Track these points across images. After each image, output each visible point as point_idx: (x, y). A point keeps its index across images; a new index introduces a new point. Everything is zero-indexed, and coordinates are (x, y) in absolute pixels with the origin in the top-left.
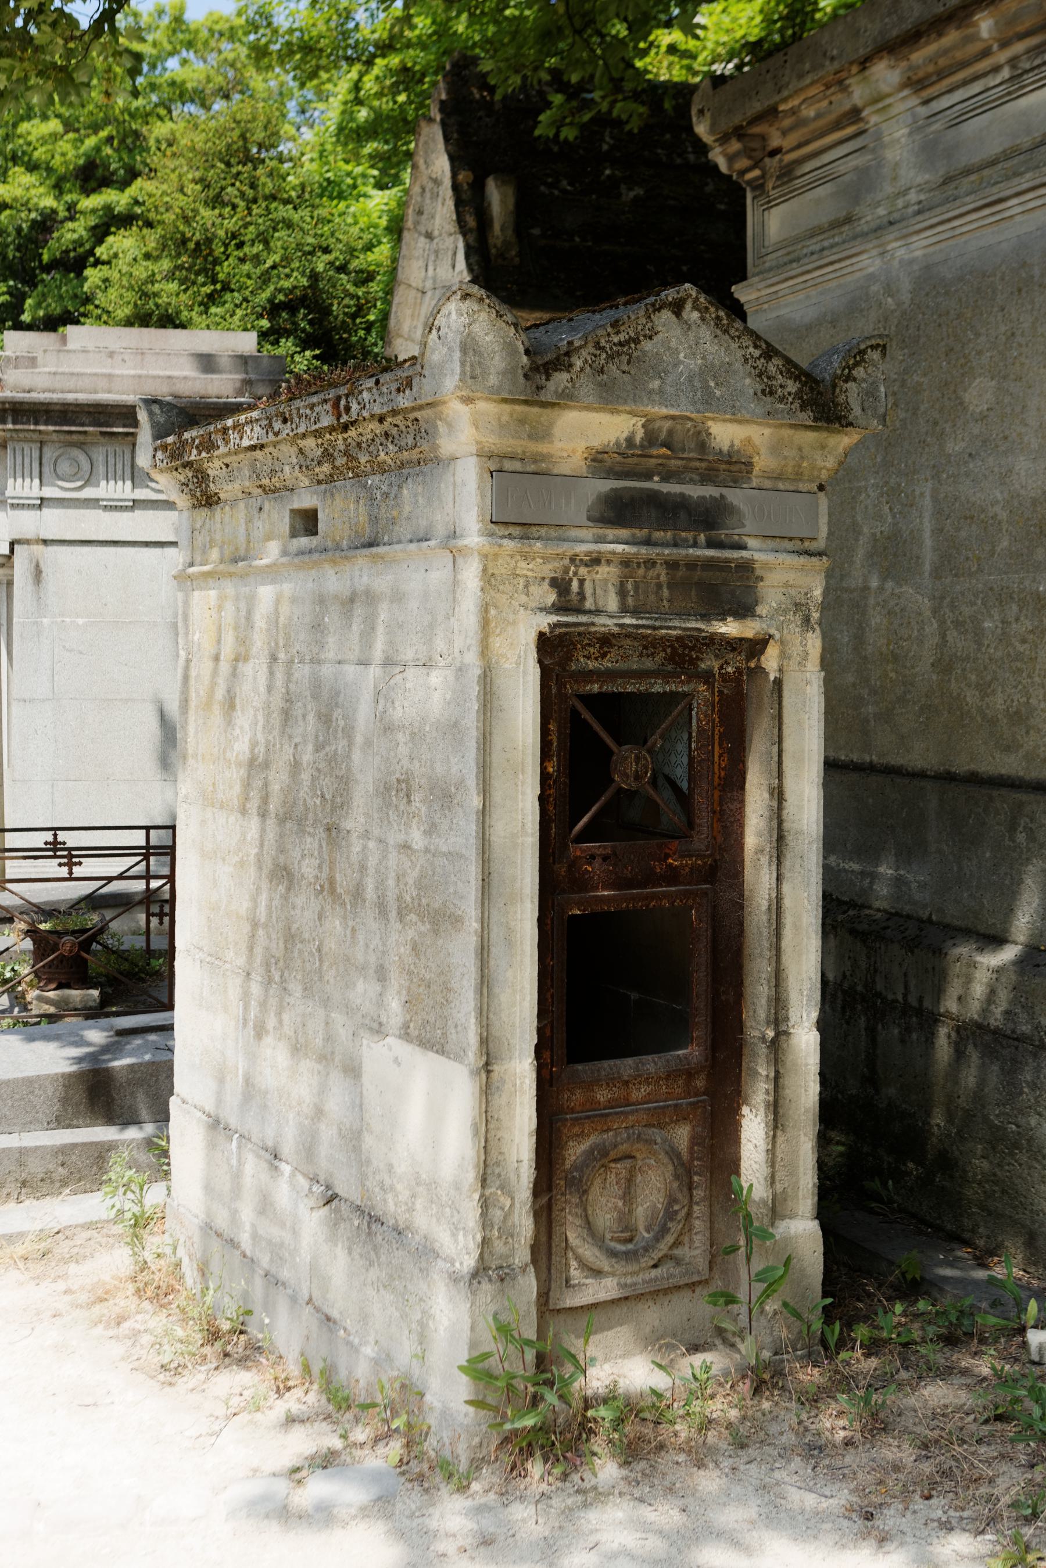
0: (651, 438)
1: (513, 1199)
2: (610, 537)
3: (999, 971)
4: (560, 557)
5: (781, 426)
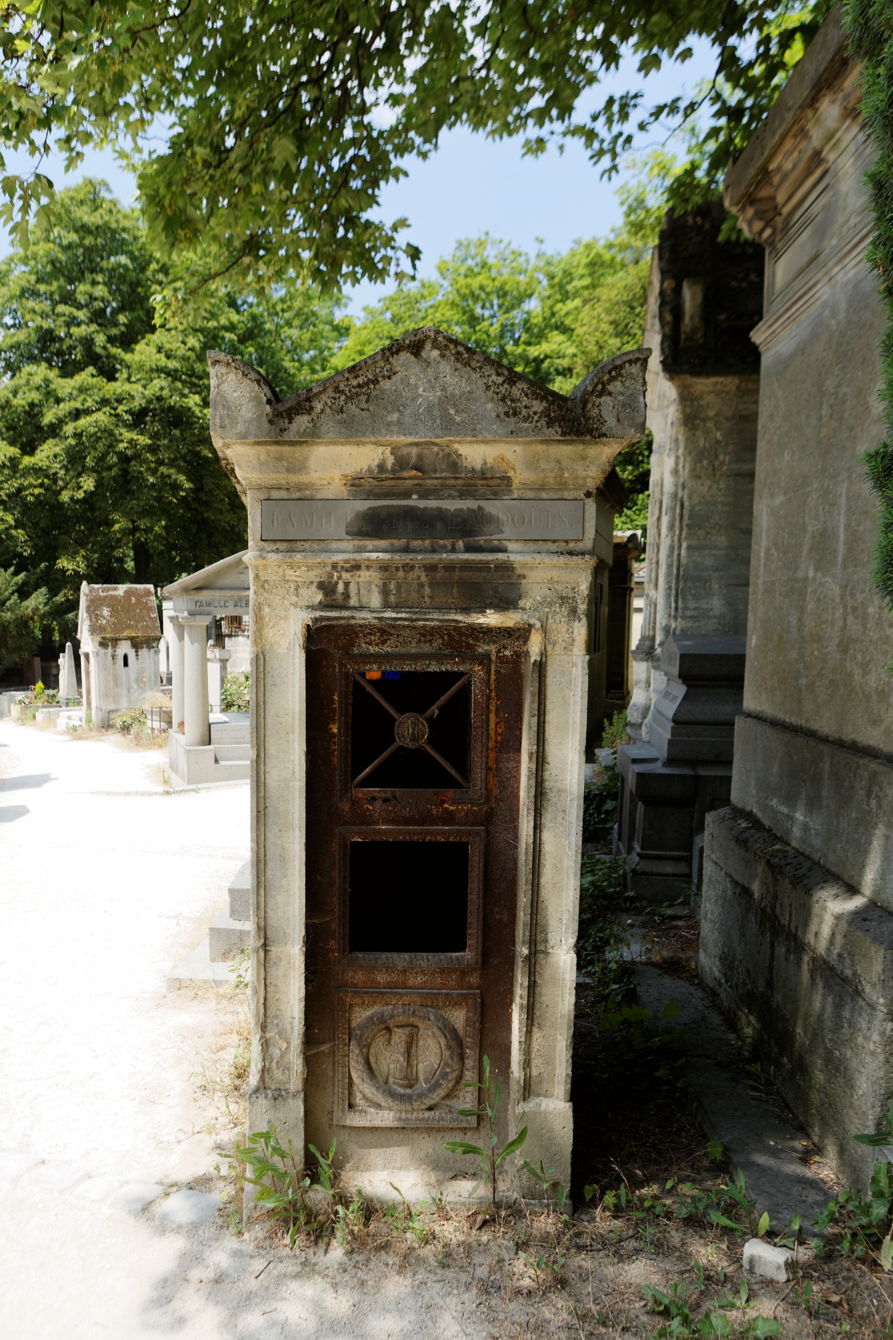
0: (402, 463)
1: (288, 1043)
2: (370, 547)
3: (838, 917)
4: (322, 564)
5: (531, 442)
